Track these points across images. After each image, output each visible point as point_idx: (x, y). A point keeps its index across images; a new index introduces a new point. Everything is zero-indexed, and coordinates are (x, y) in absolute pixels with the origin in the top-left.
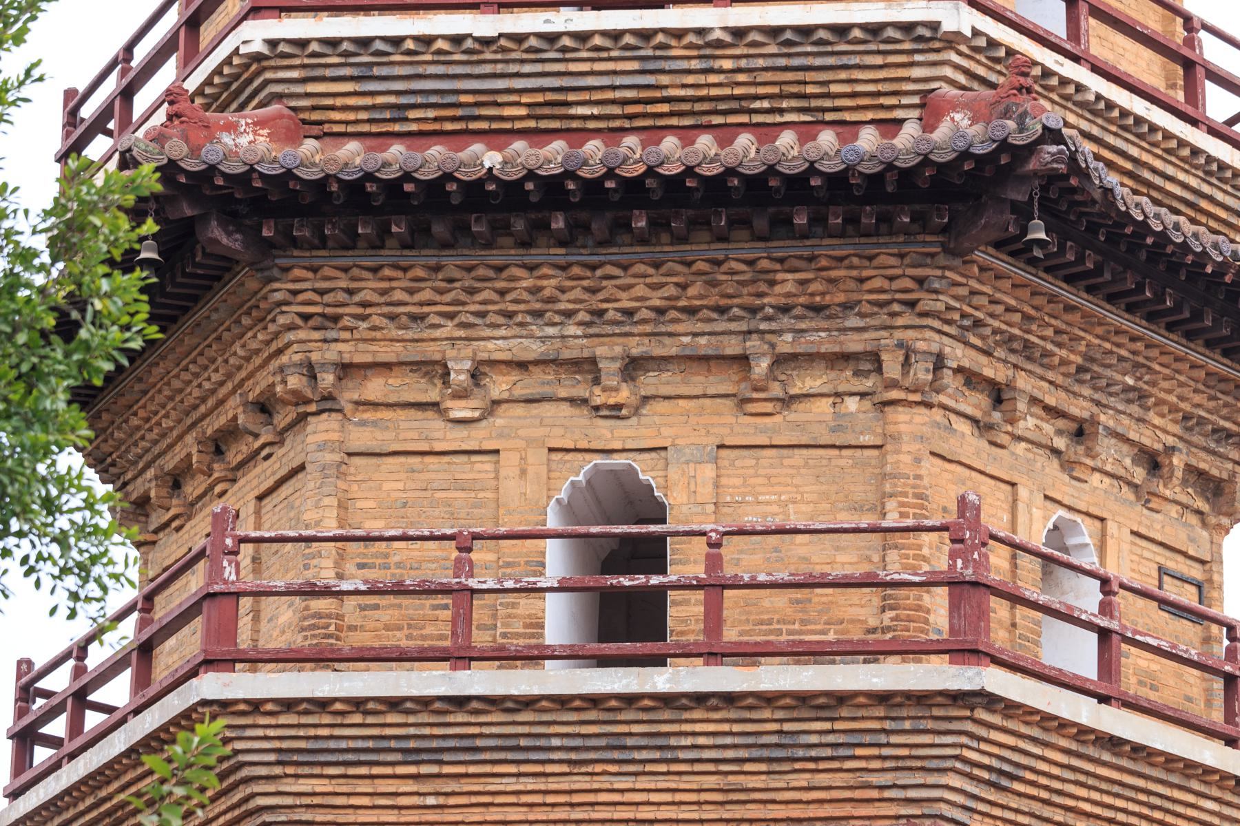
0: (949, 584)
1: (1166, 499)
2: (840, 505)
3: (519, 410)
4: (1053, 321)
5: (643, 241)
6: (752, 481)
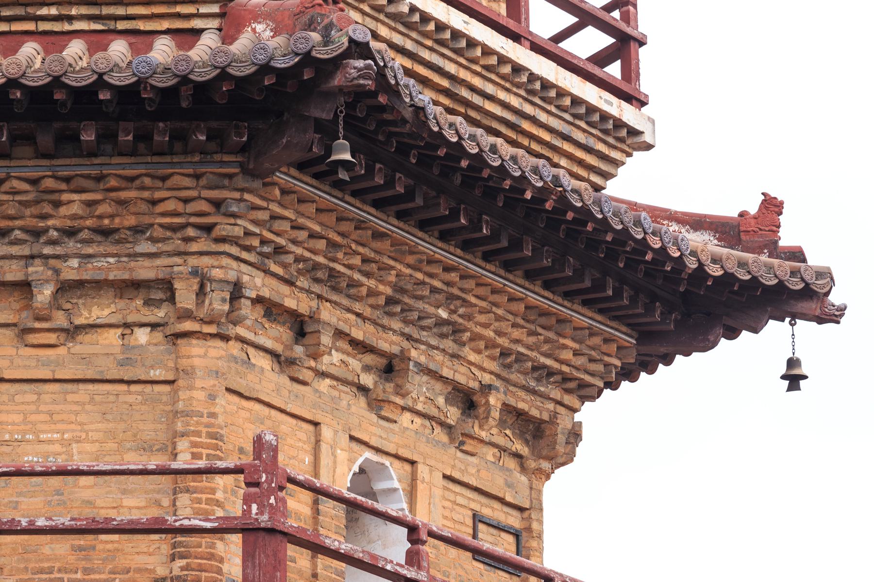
1: (482, 441)
2: (128, 445)
4: (361, 249)
6: (33, 418)
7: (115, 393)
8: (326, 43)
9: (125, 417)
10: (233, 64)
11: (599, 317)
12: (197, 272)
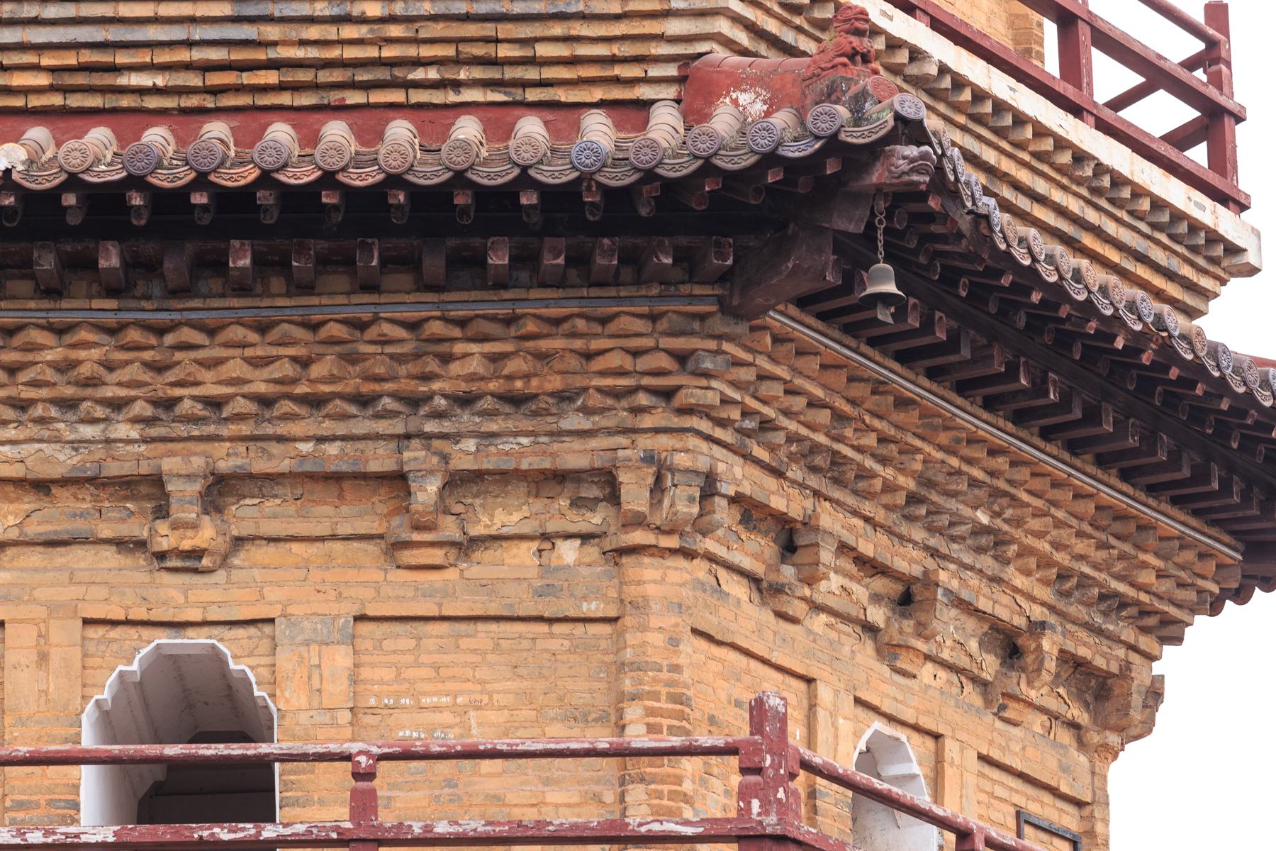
0: (739, 839)
1: (1030, 704)
2: (552, 713)
3: (35, 558)
4: (877, 423)
5: (242, 289)
6: (410, 673)
7: (531, 636)
8: (857, 122)
9: (545, 672)
10: (722, 152)
11: (1194, 522)
12: (653, 458)
